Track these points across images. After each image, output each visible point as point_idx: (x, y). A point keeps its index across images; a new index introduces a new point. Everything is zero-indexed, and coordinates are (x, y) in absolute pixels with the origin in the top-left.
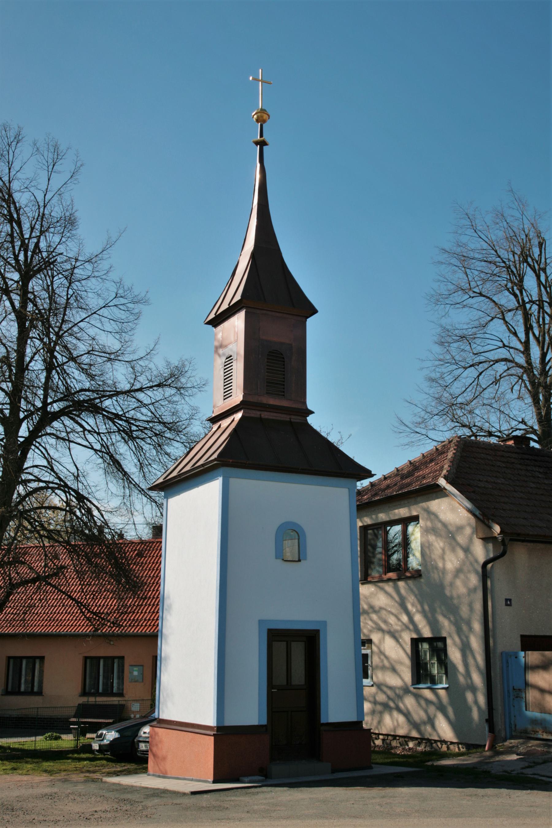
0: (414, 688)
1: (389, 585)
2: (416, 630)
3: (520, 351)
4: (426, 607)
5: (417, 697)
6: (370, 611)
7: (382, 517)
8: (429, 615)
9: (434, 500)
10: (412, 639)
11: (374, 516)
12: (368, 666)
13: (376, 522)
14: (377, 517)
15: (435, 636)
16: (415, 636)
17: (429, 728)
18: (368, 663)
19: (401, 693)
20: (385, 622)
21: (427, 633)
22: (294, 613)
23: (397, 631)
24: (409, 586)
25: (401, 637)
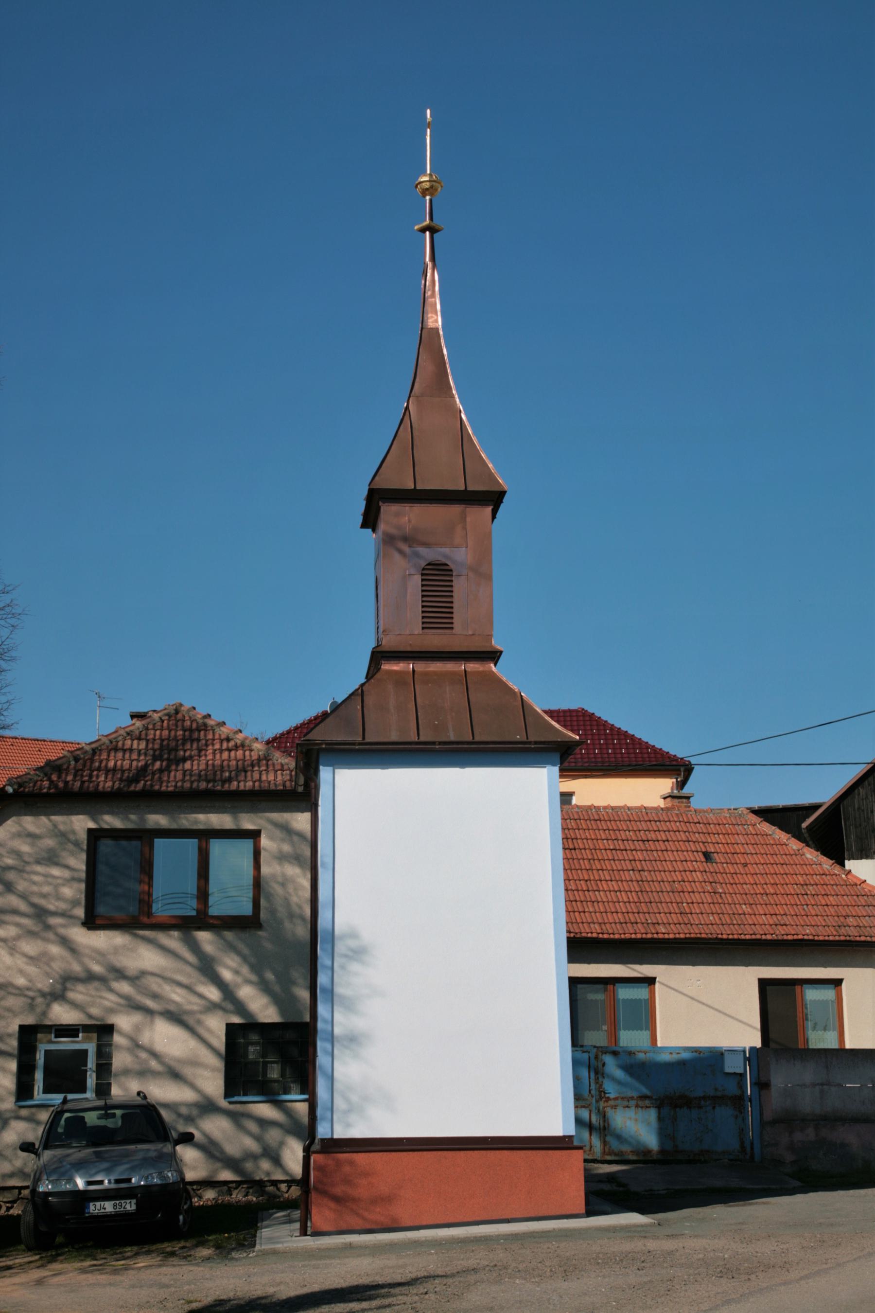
0: (230, 1103)
1: (170, 936)
2: (240, 1007)
3: (761, 1114)
4: (270, 976)
5: (235, 1117)
6: (111, 976)
7: (158, 820)
8: (277, 988)
9: (302, 812)
10: (230, 1027)
11: (133, 817)
12: (86, 1071)
13: (141, 827)
14: (143, 820)
15: (290, 1020)
16: (236, 1020)
17: (266, 1165)
18: (86, 1066)
19: (195, 1112)
20: (155, 996)
21: (265, 1011)
22: (576, 1193)
23: (191, 1013)
24: (225, 940)
25: (199, 1022)
